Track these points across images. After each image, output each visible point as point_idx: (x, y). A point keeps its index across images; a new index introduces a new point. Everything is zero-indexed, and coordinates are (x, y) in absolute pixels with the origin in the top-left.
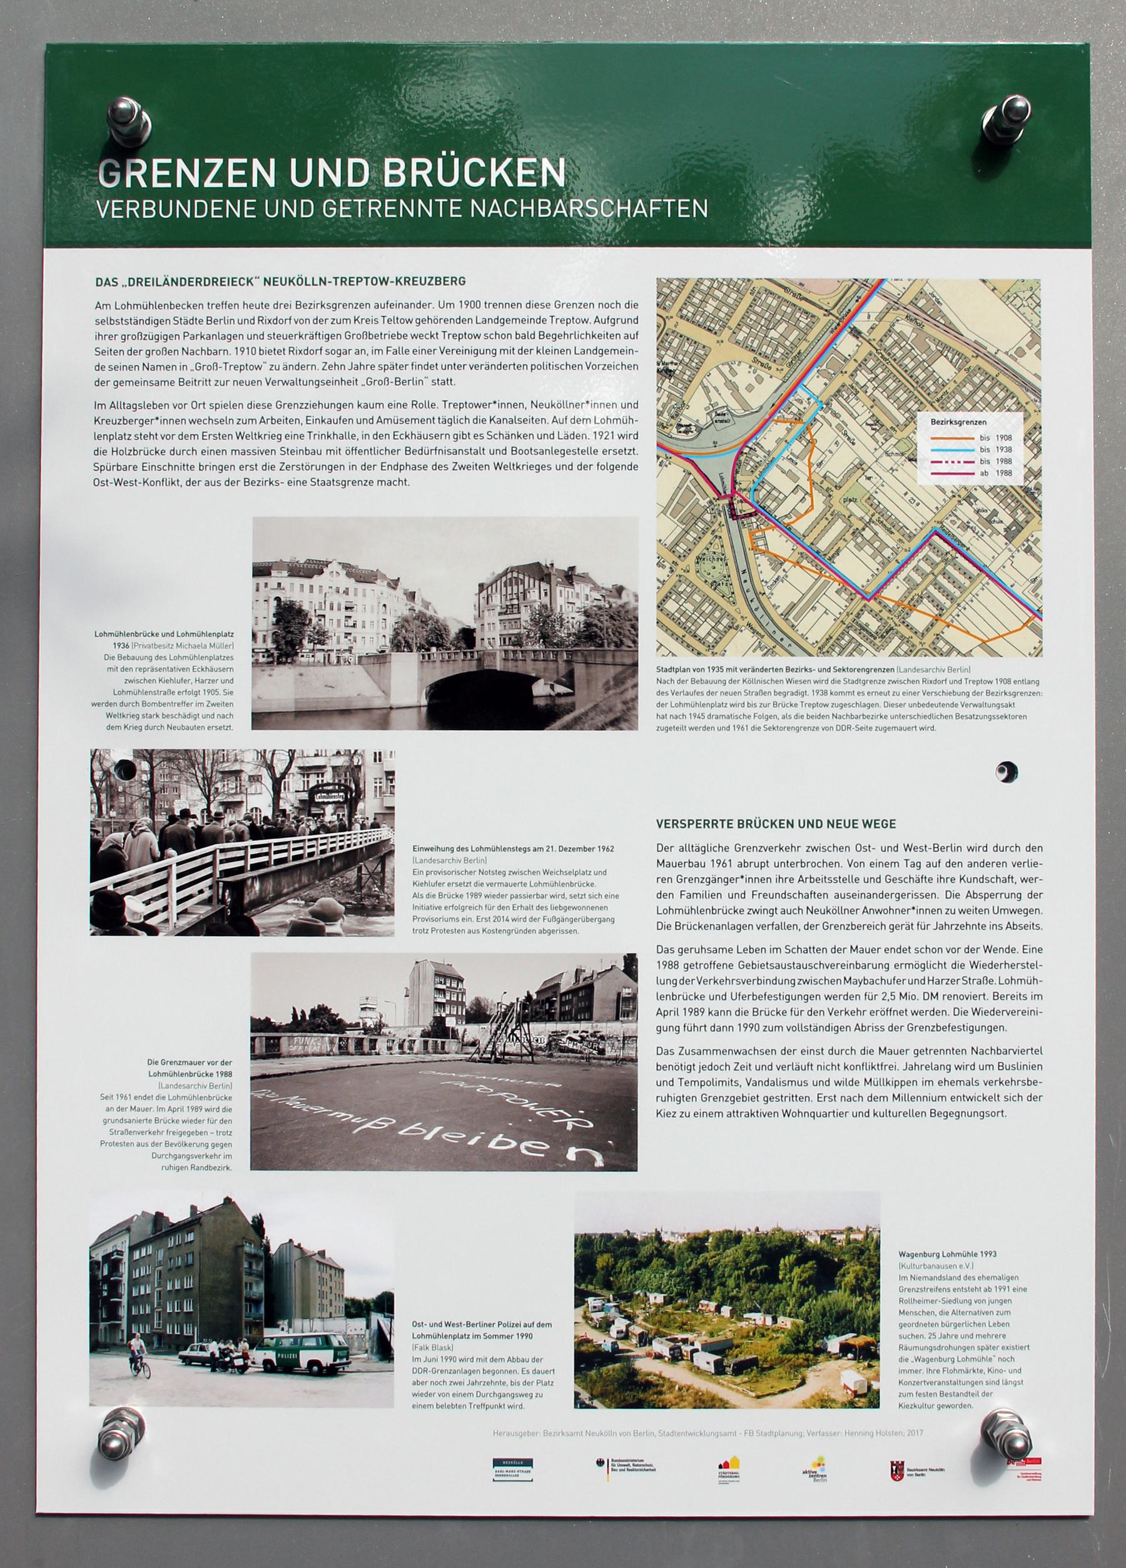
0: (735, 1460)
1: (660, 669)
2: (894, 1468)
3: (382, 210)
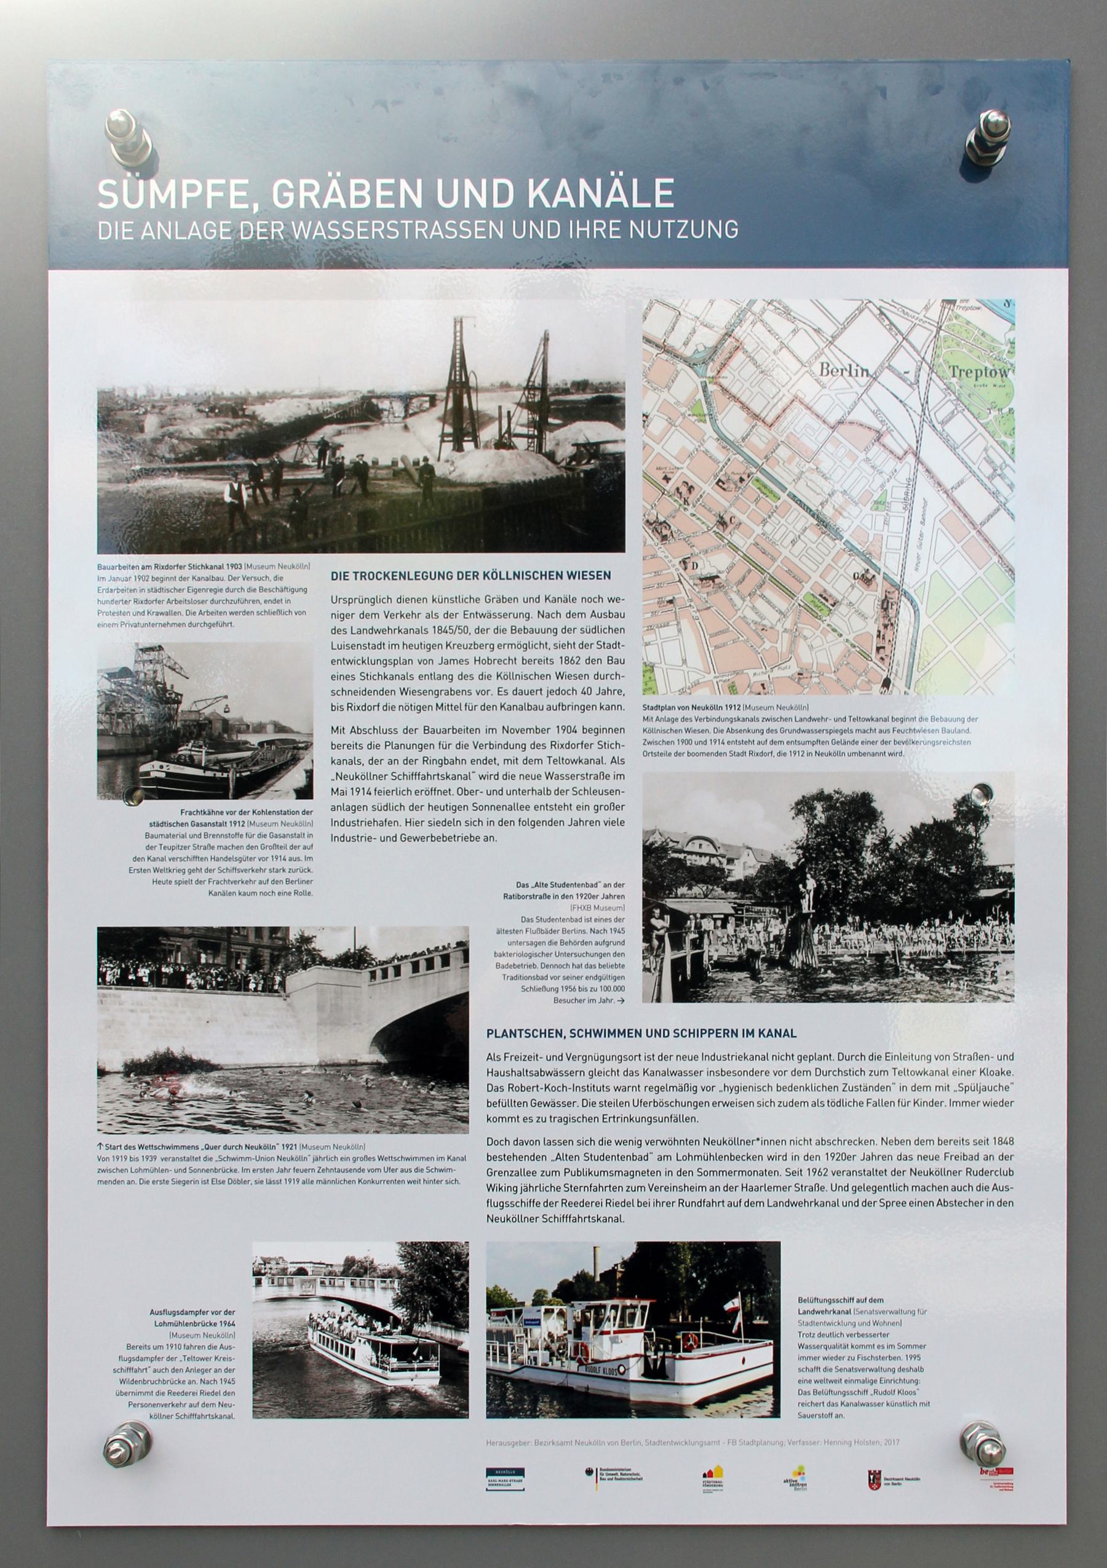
0: (719, 1469)
1: (646, 707)
2: (872, 1477)
3: (607, 231)
